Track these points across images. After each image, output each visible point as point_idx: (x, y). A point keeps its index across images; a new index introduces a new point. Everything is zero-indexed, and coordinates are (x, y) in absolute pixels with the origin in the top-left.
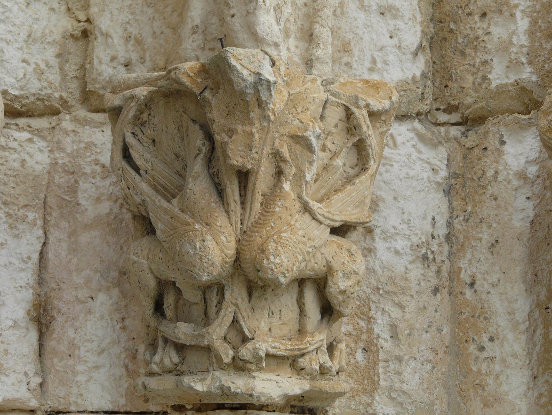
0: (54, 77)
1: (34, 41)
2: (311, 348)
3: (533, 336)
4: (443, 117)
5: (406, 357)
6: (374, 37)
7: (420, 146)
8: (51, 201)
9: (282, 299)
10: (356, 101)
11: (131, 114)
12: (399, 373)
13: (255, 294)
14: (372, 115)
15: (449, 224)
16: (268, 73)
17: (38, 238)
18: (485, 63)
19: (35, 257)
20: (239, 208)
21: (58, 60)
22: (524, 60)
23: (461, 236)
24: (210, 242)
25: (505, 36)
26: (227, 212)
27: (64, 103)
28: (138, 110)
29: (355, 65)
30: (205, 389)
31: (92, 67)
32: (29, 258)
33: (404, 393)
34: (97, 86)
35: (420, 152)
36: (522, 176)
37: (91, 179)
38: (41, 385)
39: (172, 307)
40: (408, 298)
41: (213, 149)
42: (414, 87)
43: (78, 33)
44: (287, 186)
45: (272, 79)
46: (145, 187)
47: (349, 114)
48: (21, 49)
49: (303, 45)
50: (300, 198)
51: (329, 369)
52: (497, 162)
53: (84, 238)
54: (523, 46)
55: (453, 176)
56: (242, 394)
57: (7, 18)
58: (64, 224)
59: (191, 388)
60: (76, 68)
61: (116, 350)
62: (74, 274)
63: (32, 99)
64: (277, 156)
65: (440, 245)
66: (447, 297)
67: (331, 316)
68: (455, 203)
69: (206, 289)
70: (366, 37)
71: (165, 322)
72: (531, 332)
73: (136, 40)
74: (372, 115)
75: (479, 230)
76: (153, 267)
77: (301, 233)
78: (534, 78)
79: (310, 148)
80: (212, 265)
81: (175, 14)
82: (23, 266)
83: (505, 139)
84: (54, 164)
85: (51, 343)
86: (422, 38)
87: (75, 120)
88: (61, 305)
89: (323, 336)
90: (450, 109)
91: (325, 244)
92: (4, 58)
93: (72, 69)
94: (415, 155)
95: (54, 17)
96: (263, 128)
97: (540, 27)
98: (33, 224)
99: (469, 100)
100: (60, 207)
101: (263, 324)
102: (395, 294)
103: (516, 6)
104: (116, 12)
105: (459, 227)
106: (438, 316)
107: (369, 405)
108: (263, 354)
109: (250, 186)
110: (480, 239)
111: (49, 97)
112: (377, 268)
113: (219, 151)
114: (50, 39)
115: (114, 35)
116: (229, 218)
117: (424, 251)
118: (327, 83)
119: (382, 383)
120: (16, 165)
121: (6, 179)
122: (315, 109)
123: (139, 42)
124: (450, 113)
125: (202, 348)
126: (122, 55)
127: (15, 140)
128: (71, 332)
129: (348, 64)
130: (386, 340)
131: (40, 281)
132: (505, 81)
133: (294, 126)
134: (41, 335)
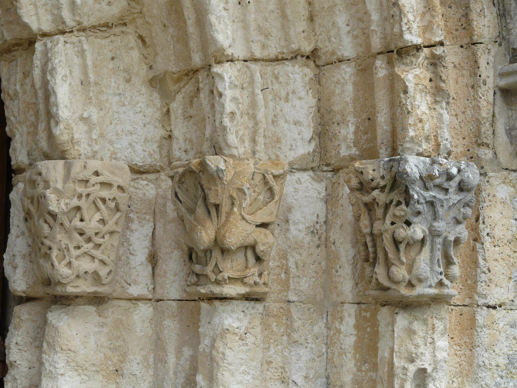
0: (157, 156)
1: (148, 141)
2: (249, 275)
3: (355, 266)
4: (325, 168)
5: (301, 276)
6: (292, 134)
7: (313, 182)
8: (157, 210)
9: (237, 254)
10: (267, 172)
11: (177, 179)
12: (299, 283)
13: (225, 253)
14: (275, 177)
15: (326, 217)
17: (151, 226)
18: (339, 145)
19: (150, 234)
24: (204, 234)
27: (161, 167)
29: (283, 148)
31: (172, 152)
33: (301, 291)
35: (313, 185)
38: (154, 289)
40: (304, 250)
42: (308, 157)
43: (167, 136)
44: (235, 209)
46: (183, 209)
47: (264, 177)
48: (142, 145)
49: (252, 144)
50: (241, 214)
52: (343, 189)
53: (169, 227)
54: (351, 139)
56: (218, 294)
57: (136, 132)
58: (162, 220)
59: (199, 291)
61: (182, 274)
63: (148, 166)
64: (231, 197)
65: (320, 226)
66: (324, 249)
68: (329, 207)
73: (189, 140)
77: (241, 228)
78: (357, 153)
79: (245, 194)
82: (145, 239)
84: (157, 194)
85: (157, 271)
86: (313, 134)
88: (161, 255)
90: (328, 165)
91: (253, 232)
93: (165, 152)
94: (310, 186)
95: (156, 130)
96: (222, 187)
97: (360, 130)
98: (149, 220)
103: (349, 121)
104: (181, 128)
106: (319, 257)
107: (287, 296)
108: (226, 278)
110: (337, 224)
111: (155, 165)
112: (291, 238)
114: (155, 140)
117: (312, 229)
119: (291, 287)
120: (141, 195)
121: (137, 202)
122: (249, 176)
126: (183, 147)
128: (164, 267)
129: (279, 148)
130: (293, 269)
131: (153, 245)
133: (238, 183)
134: (153, 269)
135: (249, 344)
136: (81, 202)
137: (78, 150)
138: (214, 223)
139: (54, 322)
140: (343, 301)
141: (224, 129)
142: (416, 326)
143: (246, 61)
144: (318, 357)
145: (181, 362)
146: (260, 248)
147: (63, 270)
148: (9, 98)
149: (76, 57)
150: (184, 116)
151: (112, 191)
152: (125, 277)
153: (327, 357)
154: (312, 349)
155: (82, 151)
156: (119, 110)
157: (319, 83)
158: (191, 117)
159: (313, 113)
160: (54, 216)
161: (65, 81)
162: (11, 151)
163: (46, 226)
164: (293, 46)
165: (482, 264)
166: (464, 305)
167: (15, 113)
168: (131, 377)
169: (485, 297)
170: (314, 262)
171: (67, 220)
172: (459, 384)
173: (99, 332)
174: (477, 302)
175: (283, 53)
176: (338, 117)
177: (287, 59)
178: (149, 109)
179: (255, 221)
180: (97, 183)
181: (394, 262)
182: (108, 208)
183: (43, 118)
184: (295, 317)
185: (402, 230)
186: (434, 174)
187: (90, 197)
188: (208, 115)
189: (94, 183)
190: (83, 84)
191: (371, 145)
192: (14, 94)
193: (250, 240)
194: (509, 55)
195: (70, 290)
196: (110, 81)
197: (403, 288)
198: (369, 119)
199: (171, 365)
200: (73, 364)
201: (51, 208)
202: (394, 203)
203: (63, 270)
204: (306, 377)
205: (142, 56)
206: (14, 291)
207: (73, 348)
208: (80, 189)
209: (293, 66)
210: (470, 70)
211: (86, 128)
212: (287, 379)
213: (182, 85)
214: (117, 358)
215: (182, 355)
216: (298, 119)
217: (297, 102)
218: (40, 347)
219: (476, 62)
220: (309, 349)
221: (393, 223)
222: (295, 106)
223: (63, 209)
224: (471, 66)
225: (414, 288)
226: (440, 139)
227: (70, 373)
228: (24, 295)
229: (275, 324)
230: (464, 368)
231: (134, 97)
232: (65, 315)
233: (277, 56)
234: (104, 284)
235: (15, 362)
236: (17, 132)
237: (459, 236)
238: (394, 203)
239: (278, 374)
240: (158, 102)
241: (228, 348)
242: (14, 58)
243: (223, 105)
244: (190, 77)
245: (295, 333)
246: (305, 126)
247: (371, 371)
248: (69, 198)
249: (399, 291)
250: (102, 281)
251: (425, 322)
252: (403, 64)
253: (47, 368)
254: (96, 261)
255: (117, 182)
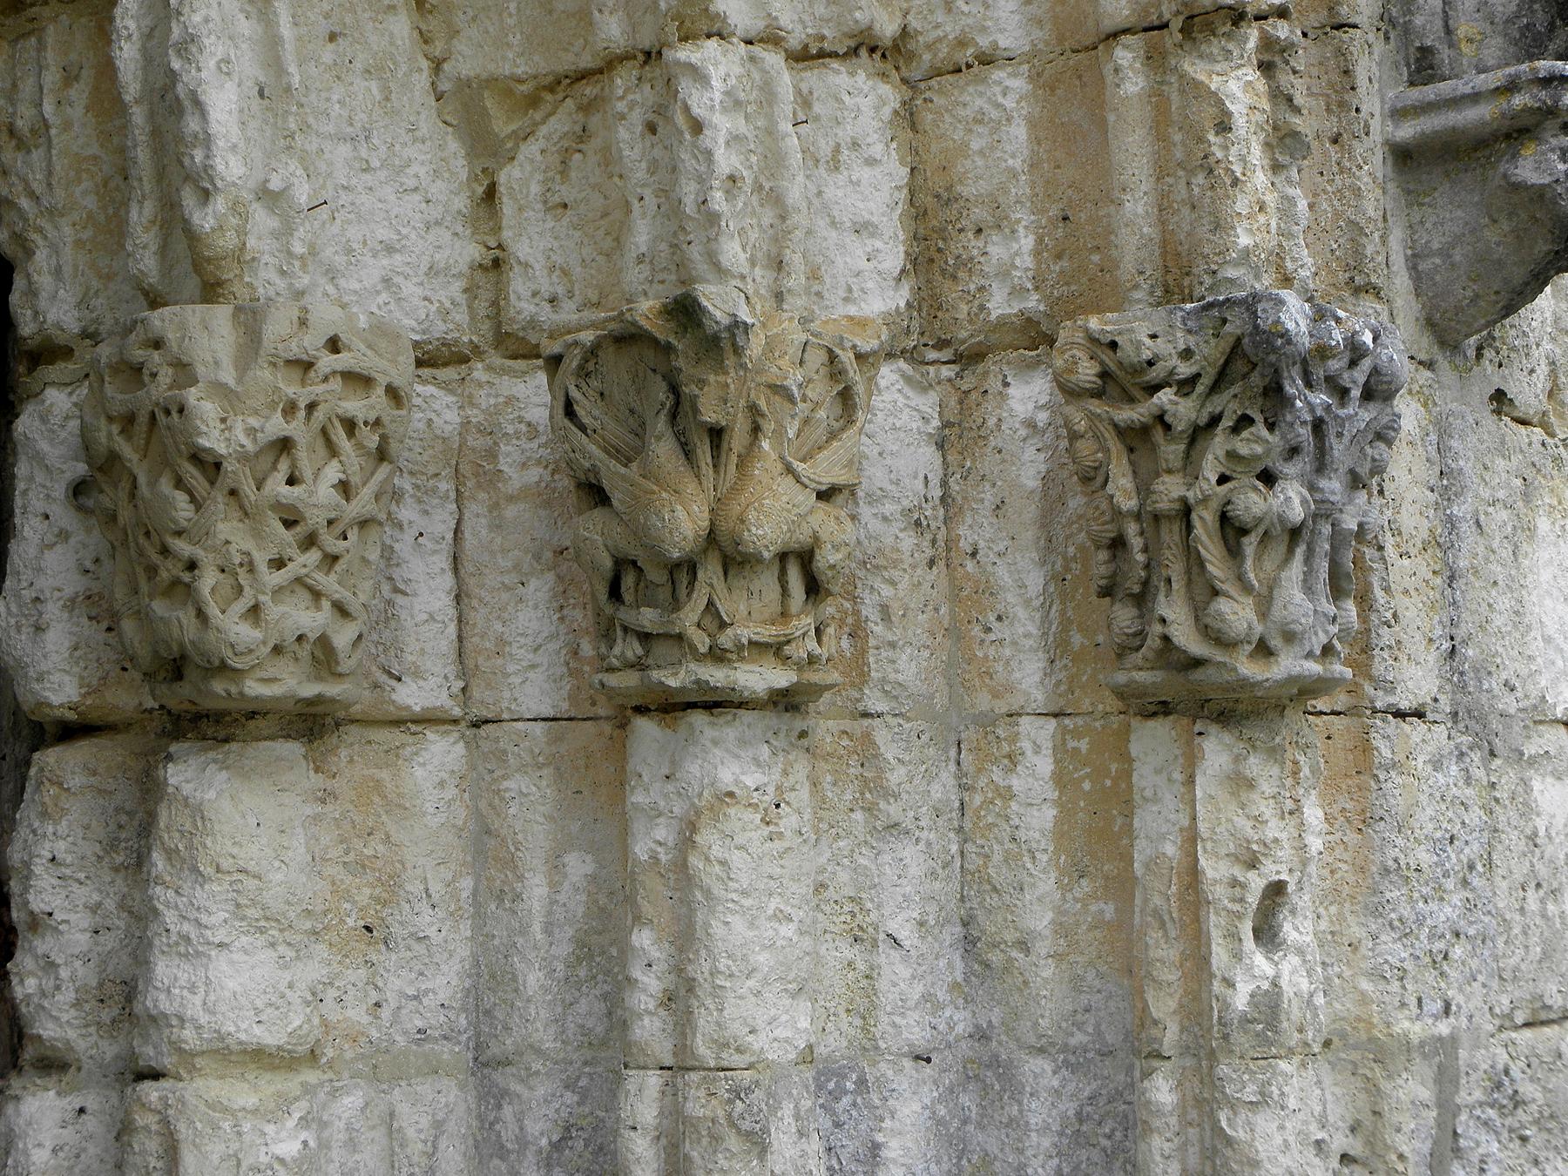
0: (461, 316)
2: (797, 634)
3: (1047, 616)
4: (932, 355)
6: (848, 260)
8: (465, 469)
11: (575, 364)
14: (860, 357)
15: (944, 484)
16: (745, 315)
18: (981, 289)
19: (449, 536)
20: (711, 471)
21: (465, 296)
22: (1029, 286)
23: (959, 498)
25: (1005, 257)
26: (698, 476)
28: (582, 358)
29: (826, 295)
30: (678, 685)
32: (443, 538)
33: (900, 684)
34: (515, 327)
36: (1031, 424)
37: (514, 441)
38: (464, 690)
39: (632, 590)
41: (677, 403)
43: (487, 262)
44: (766, 445)
45: (749, 321)
47: (832, 357)
48: (421, 284)
50: (782, 458)
51: (819, 657)
53: (510, 512)
55: (947, 425)
56: (723, 689)
58: (482, 495)
60: (487, 304)
61: (553, 646)
62: (499, 555)
64: (753, 409)
67: (817, 594)
69: (674, 568)
70: (839, 261)
71: (622, 608)
72: (1046, 608)
73: (562, 269)
74: (860, 357)
75: (980, 489)
76: (610, 543)
77: (785, 499)
78: (1042, 308)
79: (791, 399)
80: (685, 539)
81: (609, 239)
83: (1009, 379)
84: (466, 423)
87: (489, 368)
89: (810, 620)
90: (941, 344)
92: (402, 296)
93: (482, 307)
94: (901, 401)
95: (458, 244)
97: (1047, 245)
99: (963, 334)
100: (476, 475)
101: (742, 607)
102: (886, 568)
103: (1018, 221)
105: (957, 488)
109: (725, 446)
113: (686, 406)
115: (537, 266)
116: (700, 484)
118: (804, 321)
122: (794, 352)
123: (565, 273)
124: (941, 350)
125: (671, 636)
126: (546, 289)
127: (419, 395)
129: (818, 294)
130: (876, 624)
132: (1008, 311)
135: (788, 834)
136: (294, 424)
137: (250, 285)
138: (705, 483)
139: (187, 789)
140: (1015, 708)
141: (713, 219)
142: (1254, 768)
143: (751, 43)
144: (943, 868)
145: (562, 898)
146: (827, 558)
147: (234, 629)
148: (13, 143)
149: (241, 16)
150: (545, 202)
151: (373, 399)
152: (382, 658)
153: (962, 867)
154: (929, 844)
155: (261, 290)
156: (354, 181)
157: (914, 127)
158: (565, 206)
159: (900, 205)
160: (212, 466)
161: (228, 74)
162: (15, 298)
163: (181, 498)
164: (858, 15)
165: (1382, 601)
166: (1334, 713)
167: (35, 185)
168: (412, 942)
169: (1390, 686)
170: (925, 606)
171: (251, 481)
172: (1332, 922)
173: (317, 819)
174: (1372, 702)
175: (823, 38)
176: (979, 213)
177: (833, 55)
178: (439, 182)
180: (334, 372)
181: (1224, 587)
182: (360, 446)
183: (147, 187)
184: (889, 756)
185: (1253, 496)
186: (1334, 343)
187: (316, 414)
188: (639, 190)
189: (328, 370)
190: (266, 93)
191: (1073, 288)
192: (32, 130)
193: (803, 537)
194: (1408, 65)
195: (253, 688)
196: (328, 100)
197: (1245, 660)
198: (1065, 219)
199: (536, 906)
200: (252, 913)
201: (203, 442)
202: (1227, 422)
203: (237, 628)
204: (921, 924)
205: (416, 33)
206: (40, 704)
207: (252, 866)
208: (291, 389)
209: (852, 74)
210: (1328, 95)
211: (273, 223)
212: (870, 929)
213: (538, 116)
214: (367, 891)
215: (565, 876)
216: (867, 217)
217: (864, 174)
218: (140, 861)
219: (1346, 72)
220: (922, 846)
221: (1222, 480)
222: (858, 183)
223: (243, 446)
224: (1331, 85)
225: (1272, 659)
226: (1289, 264)
227: (244, 939)
228: (72, 716)
229: (829, 778)
230: (1342, 878)
231: (398, 147)
232: (221, 769)
233: (806, 46)
234: (340, 675)
235: (50, 914)
236: (40, 242)
238: (1227, 422)
239: (843, 918)
240: (461, 167)
241: (737, 848)
242: (30, 26)
243: (709, 154)
244: (560, 96)
245: (892, 800)
246: (886, 238)
247: (1098, 899)
248: (256, 412)
249: (1235, 669)
250: (337, 663)
251: (1275, 753)
252: (1201, 57)
253: (172, 927)
254: (326, 604)
255: (384, 373)
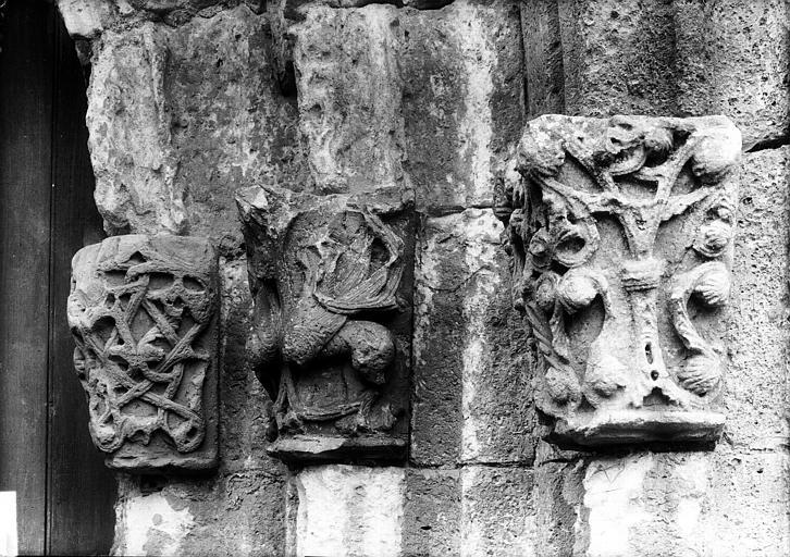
179: (341, 306)
180: (141, 275)
182: (169, 317)
237: (699, 288)
254: (160, 412)
